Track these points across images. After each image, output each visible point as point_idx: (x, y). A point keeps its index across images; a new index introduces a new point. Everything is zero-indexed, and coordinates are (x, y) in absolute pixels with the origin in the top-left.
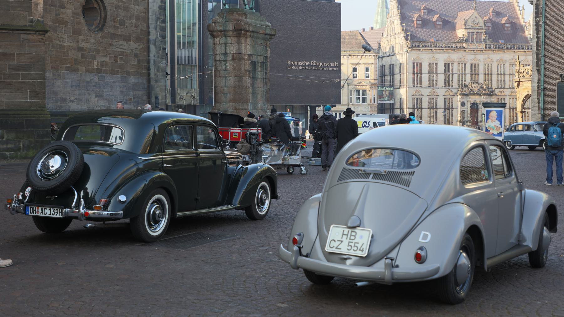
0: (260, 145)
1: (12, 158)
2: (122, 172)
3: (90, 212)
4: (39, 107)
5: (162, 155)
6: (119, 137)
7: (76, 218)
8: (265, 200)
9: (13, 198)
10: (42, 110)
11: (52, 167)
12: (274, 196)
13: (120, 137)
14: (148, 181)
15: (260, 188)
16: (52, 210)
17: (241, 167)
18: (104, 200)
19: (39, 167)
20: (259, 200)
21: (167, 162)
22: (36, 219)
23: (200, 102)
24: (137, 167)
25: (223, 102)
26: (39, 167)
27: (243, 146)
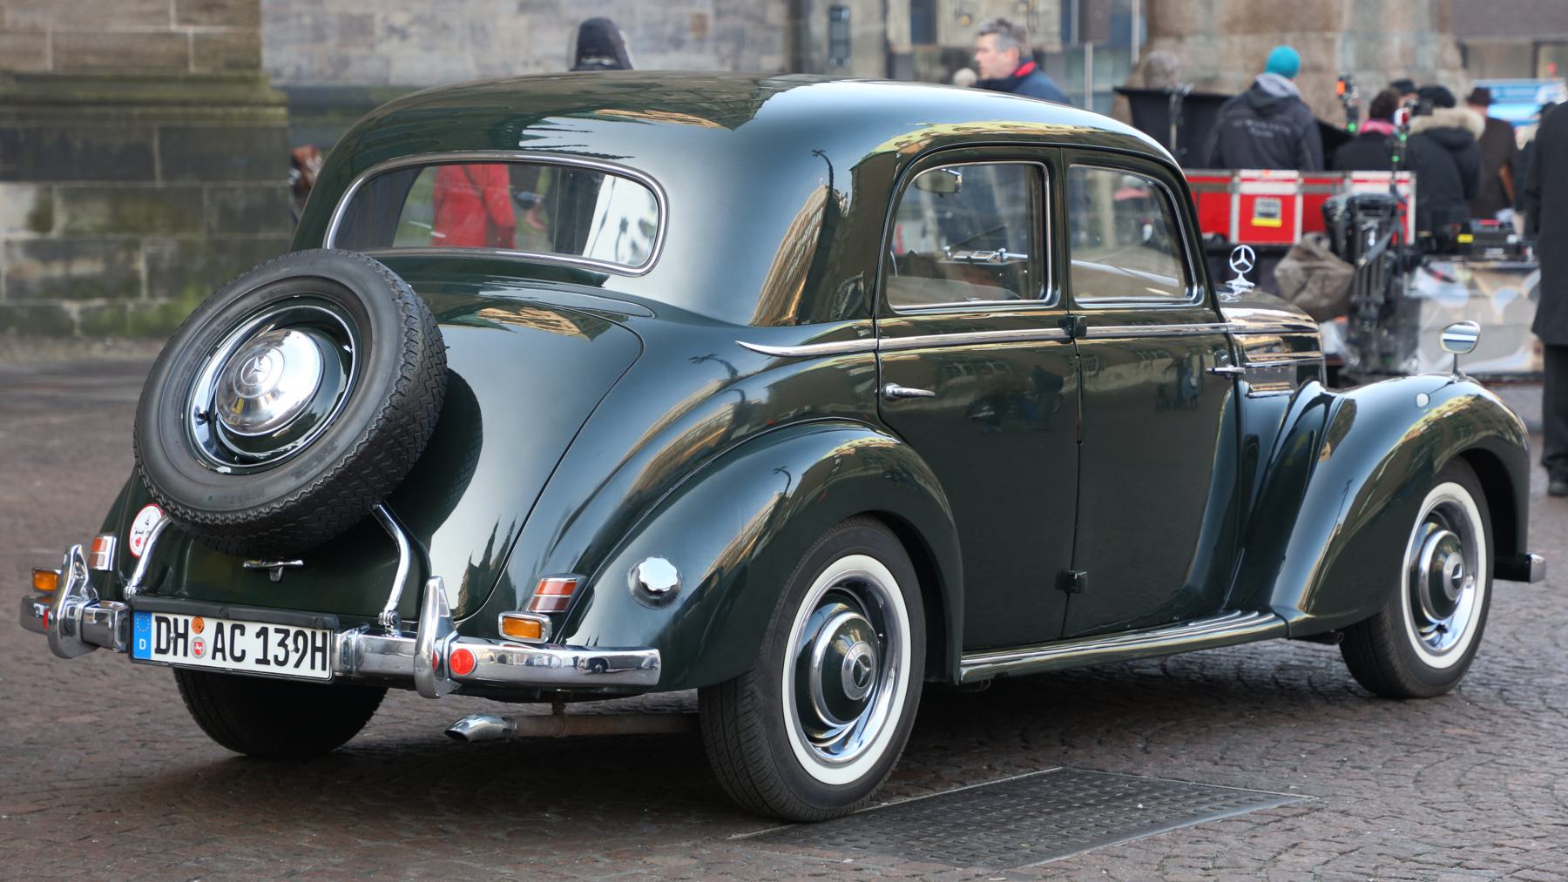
0: (1409, 265)
1: (96, 330)
2: (647, 432)
3: (480, 651)
4: (232, 65)
5: (874, 332)
6: (647, 231)
7: (406, 681)
8: (1457, 584)
9: (65, 568)
10: (244, 81)
11: (275, 394)
12: (1510, 563)
13: (643, 225)
14: (797, 480)
15: (1430, 517)
16: (274, 638)
17: (1324, 399)
18: (551, 591)
19: (201, 399)
20: (1425, 583)
21: (899, 371)
22: (193, 681)
23: (1065, 35)
24: (735, 398)
25: (1194, 33)
26: (201, 399)
27: (1309, 271)
